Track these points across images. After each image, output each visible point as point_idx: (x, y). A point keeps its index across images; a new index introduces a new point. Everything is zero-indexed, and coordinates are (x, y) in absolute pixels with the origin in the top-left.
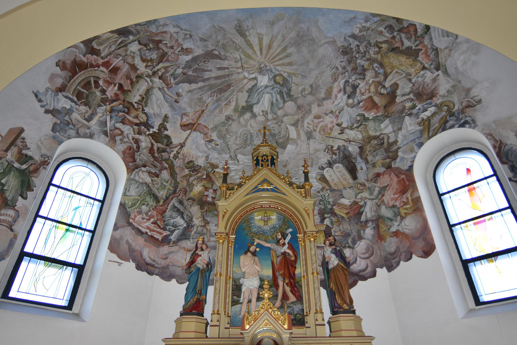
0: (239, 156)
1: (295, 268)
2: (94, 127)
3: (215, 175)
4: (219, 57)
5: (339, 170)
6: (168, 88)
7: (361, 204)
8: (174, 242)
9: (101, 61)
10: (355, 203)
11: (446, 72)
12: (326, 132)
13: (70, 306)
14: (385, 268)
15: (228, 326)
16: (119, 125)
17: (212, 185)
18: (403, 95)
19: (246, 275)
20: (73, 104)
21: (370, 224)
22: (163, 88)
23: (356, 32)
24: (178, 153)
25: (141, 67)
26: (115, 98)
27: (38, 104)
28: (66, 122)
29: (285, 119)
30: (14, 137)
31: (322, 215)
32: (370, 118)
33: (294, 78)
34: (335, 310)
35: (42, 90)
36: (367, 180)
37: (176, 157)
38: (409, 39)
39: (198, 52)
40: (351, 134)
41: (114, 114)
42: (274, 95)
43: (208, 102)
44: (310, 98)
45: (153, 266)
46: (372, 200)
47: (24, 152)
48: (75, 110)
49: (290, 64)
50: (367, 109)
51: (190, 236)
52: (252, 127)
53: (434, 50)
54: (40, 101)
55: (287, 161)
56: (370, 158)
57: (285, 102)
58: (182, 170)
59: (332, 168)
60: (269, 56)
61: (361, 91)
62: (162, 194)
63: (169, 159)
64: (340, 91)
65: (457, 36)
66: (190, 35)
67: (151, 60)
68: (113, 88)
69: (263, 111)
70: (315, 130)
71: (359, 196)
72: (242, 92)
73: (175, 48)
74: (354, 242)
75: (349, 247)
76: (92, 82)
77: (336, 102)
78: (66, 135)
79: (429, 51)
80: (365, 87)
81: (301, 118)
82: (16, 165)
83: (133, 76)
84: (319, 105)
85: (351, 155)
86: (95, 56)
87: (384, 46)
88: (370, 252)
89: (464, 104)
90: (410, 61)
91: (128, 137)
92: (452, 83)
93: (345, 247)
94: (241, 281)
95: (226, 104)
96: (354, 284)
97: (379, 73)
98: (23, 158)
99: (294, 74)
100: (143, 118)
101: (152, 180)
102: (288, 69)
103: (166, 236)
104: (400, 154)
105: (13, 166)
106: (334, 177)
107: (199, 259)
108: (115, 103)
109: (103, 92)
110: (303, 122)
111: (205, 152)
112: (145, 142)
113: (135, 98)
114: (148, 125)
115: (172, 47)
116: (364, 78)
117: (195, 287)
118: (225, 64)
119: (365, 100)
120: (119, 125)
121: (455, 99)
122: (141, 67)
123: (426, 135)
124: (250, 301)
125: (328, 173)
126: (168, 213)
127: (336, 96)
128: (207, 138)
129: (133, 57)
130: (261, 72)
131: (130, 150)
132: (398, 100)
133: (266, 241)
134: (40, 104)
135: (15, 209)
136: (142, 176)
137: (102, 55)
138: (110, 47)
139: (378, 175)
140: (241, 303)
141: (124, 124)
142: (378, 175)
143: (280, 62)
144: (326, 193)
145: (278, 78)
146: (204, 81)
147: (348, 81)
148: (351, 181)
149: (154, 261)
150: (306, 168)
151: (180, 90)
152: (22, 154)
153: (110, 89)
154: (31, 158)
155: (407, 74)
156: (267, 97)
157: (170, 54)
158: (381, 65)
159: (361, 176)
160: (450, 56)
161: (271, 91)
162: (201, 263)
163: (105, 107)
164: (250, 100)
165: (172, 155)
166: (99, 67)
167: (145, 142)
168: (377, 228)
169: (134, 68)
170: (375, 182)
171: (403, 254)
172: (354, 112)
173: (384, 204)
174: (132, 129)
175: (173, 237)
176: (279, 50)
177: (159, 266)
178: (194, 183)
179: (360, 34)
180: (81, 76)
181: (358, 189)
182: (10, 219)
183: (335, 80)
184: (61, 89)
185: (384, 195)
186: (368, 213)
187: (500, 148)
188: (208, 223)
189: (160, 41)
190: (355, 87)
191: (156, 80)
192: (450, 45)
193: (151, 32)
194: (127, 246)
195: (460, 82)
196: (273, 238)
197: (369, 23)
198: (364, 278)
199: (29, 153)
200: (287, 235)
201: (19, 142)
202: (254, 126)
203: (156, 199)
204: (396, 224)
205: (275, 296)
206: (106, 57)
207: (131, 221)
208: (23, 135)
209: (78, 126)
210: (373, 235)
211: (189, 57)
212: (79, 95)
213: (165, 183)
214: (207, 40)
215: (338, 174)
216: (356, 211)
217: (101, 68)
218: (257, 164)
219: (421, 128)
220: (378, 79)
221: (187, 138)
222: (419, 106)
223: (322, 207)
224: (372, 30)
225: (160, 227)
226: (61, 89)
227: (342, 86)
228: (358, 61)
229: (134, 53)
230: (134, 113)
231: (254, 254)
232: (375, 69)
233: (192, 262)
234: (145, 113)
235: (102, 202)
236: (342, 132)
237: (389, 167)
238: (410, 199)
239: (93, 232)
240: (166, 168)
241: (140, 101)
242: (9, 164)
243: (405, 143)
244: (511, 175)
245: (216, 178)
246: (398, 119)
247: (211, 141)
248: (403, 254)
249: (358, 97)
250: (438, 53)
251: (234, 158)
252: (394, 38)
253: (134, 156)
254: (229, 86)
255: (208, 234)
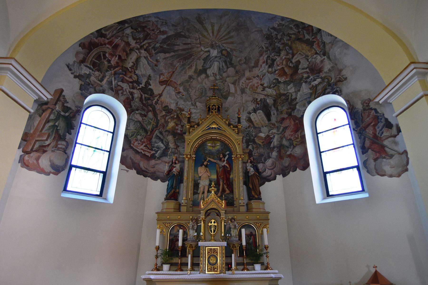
0: (198, 104)
1: (230, 175)
2: (105, 85)
3: (182, 116)
4: (185, 36)
5: (260, 114)
6: (151, 57)
7: (272, 136)
8: (158, 158)
9: (107, 41)
10: (268, 136)
11: (329, 58)
12: (253, 89)
13: (101, 195)
14: (281, 175)
15: (192, 206)
16: (120, 83)
17: (181, 122)
18: (303, 69)
19: (201, 178)
20: (91, 71)
21: (276, 149)
22: (147, 56)
23: (276, 26)
24: (158, 100)
25: (133, 43)
26: (116, 65)
27: (69, 72)
28: (87, 83)
29: (228, 79)
30: (58, 95)
31: (248, 143)
32: (282, 82)
33: (234, 52)
34: (250, 197)
35: (71, 63)
36: (277, 122)
37: (156, 103)
38: (308, 34)
39: (171, 33)
40: (269, 91)
41: (116, 76)
42: (221, 63)
43: (177, 66)
44: (244, 66)
45: (146, 172)
46: (278, 134)
47: (65, 105)
48: (92, 75)
49: (232, 43)
50: (280, 76)
51: (167, 154)
52: (206, 84)
53: (323, 43)
54: (70, 70)
55: (228, 108)
56: (279, 108)
57: (228, 68)
58: (161, 112)
59: (256, 113)
60: (218, 37)
61: (277, 63)
62: (149, 127)
63: (152, 104)
64: (264, 62)
65: (336, 38)
66: (166, 22)
67: (139, 39)
68: (115, 58)
69: (213, 73)
70: (246, 88)
71: (271, 132)
72: (200, 60)
73: (155, 30)
74: (265, 160)
75: (262, 163)
76: (102, 55)
77: (261, 70)
78: (89, 92)
79: (320, 43)
80: (280, 61)
81: (238, 79)
82: (62, 113)
83: (128, 49)
84: (250, 71)
85: (269, 105)
86: (103, 38)
87: (293, 36)
88: (274, 165)
89: (337, 79)
90: (308, 48)
91: (126, 91)
92: (332, 65)
93: (260, 163)
94: (199, 181)
95: (189, 68)
96: (263, 183)
97: (289, 53)
98: (66, 109)
99: (235, 50)
100: (135, 78)
101: (143, 119)
102: (231, 46)
103: (153, 154)
104: (297, 107)
105: (60, 114)
106: (257, 119)
107: (174, 169)
108: (116, 69)
109: (109, 61)
110: (239, 82)
111: (175, 100)
112: (137, 94)
113: (129, 65)
114: (138, 83)
115: (153, 30)
116: (280, 55)
117: (172, 185)
118: (189, 41)
119: (280, 69)
120: (120, 83)
121: (333, 75)
122: (133, 43)
123: (313, 97)
124: (203, 193)
125: (253, 116)
126: (153, 140)
127: (261, 66)
128: (177, 90)
129: (128, 37)
130: (212, 47)
131: (128, 99)
132: (300, 71)
133: (213, 158)
134: (71, 72)
135: (66, 141)
136: (137, 117)
137: (108, 37)
138: (113, 32)
139: (283, 119)
140: (199, 194)
141: (123, 82)
142: (283, 119)
143: (225, 41)
144: (251, 130)
145: (224, 52)
146: (174, 51)
147: (270, 57)
148: (267, 122)
149: (147, 169)
150: (239, 115)
151: (159, 58)
152: (65, 106)
153: (113, 59)
154: (70, 108)
155: (306, 55)
156: (216, 64)
157: (152, 34)
158: (291, 48)
159: (274, 119)
160: (332, 48)
161: (219, 60)
162: (175, 170)
163: (111, 72)
164: (205, 65)
165: (154, 102)
166: (105, 45)
167: (137, 94)
168: (279, 152)
169: (128, 44)
170: (281, 123)
171: (292, 168)
172: (272, 77)
173: (285, 138)
174: (128, 85)
175: (157, 155)
176: (225, 33)
177: (150, 172)
178: (169, 120)
179: (278, 28)
180: (95, 52)
181: (271, 127)
182: (64, 147)
183: (261, 55)
184: (83, 61)
185: (285, 132)
186: (275, 142)
187: (352, 110)
188: (179, 146)
189: (146, 27)
190: (273, 61)
191: (143, 51)
192: (332, 41)
193: (139, 21)
194: (131, 161)
195: (336, 65)
196: (218, 157)
197: (284, 22)
198: (269, 181)
199: (69, 105)
200: (226, 156)
201: (61, 99)
202: (207, 83)
203: (146, 131)
204: (290, 150)
205: (218, 190)
206: (110, 38)
207: (132, 145)
208: (63, 94)
209: (95, 86)
210: (277, 156)
211: (165, 36)
212: (94, 64)
213: (150, 121)
214: (176, 26)
215: (259, 117)
216: (268, 140)
217: (107, 46)
218: (209, 110)
219: (311, 91)
220: (288, 57)
221: (163, 91)
222: (312, 77)
223: (248, 138)
224: (286, 26)
225: (149, 149)
226: (83, 61)
227: (265, 60)
228: (277, 44)
229: (128, 35)
230: (129, 75)
231: (206, 166)
232: (286, 50)
233: (170, 171)
234: (136, 75)
235: (113, 133)
236: (264, 90)
237: (290, 114)
238: (299, 135)
239: (109, 152)
240: (151, 111)
241: (132, 66)
242: (58, 113)
243: (301, 100)
244: (355, 127)
245: (183, 117)
246: (298, 84)
247: (179, 93)
248: (292, 168)
249: (275, 67)
250: (325, 45)
251: (194, 105)
252: (299, 32)
253: (131, 104)
254: (191, 55)
255: (179, 153)
